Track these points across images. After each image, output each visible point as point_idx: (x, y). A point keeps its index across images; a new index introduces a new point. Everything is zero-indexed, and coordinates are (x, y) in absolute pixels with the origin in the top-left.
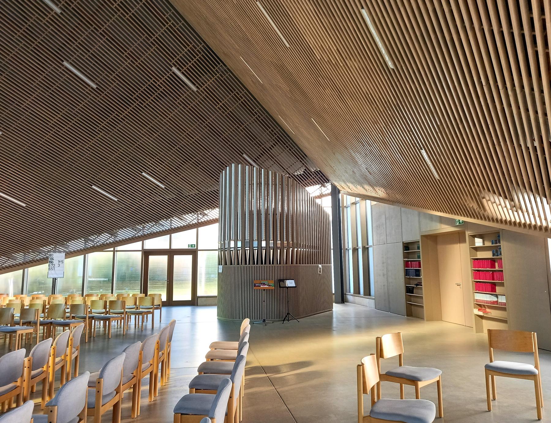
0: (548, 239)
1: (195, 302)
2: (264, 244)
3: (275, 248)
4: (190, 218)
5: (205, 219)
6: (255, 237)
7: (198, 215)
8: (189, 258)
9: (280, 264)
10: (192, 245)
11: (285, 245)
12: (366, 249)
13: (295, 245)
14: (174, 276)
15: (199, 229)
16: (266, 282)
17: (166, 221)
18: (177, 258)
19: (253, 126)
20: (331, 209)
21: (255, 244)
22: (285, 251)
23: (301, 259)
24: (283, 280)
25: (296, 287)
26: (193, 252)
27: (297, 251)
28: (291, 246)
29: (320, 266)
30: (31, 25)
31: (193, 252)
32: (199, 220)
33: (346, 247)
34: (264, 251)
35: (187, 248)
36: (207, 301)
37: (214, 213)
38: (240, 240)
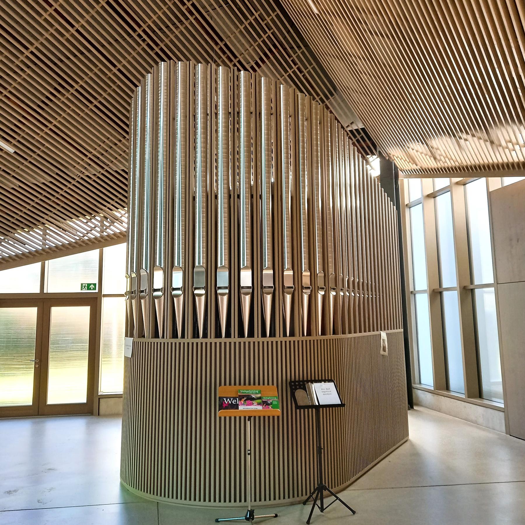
1: (92, 408)
2: (246, 278)
4: (81, 227)
6: (222, 259)
8: (83, 312)
9: (292, 334)
10: (89, 285)
11: (306, 281)
12: (468, 293)
13: (332, 284)
15: (106, 249)
16: (253, 392)
18: (57, 313)
19: (218, 14)
20: (437, 180)
23: (341, 322)
24: (300, 384)
25: (342, 405)
26: (91, 299)
28: (320, 282)
29: (384, 335)
31: (91, 299)
33: (411, 289)
34: (248, 298)
35: (79, 290)
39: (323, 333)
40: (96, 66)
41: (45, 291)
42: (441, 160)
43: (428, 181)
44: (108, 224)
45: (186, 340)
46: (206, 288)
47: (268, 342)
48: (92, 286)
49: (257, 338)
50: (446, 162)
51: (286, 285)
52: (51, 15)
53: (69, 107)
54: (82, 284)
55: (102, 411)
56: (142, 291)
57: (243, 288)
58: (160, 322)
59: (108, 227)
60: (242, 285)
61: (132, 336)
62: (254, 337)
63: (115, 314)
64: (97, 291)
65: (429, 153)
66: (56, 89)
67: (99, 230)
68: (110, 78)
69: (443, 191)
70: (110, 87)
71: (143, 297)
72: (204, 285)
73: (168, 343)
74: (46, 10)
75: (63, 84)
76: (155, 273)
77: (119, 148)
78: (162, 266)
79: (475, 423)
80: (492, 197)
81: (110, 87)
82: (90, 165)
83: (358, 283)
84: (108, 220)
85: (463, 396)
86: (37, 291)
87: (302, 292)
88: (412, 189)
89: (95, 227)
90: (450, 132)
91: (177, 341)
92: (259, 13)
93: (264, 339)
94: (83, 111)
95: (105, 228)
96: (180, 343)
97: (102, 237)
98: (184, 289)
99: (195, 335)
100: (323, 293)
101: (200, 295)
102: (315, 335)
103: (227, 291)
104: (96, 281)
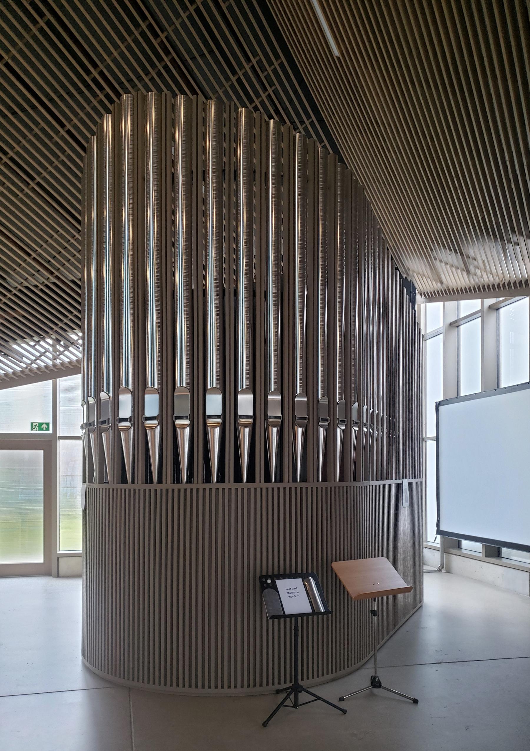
0: (277, 581)
1: (51, 568)
2: (245, 403)
10: (41, 424)
17: (33, 347)
20: (463, 303)
21: (214, 404)
22: (321, 430)
27: (358, 433)
29: (406, 482)
30: (18, 56)
38: (214, 391)
39: (342, 479)
40: (37, 124)
42: (475, 275)
44: (62, 349)
45: (163, 486)
46: (191, 417)
47: (273, 489)
48: (44, 426)
49: (260, 483)
50: (482, 277)
51: (298, 415)
54: (32, 423)
55: (61, 572)
56: (104, 422)
57: (241, 417)
59: (61, 353)
60: (240, 413)
61: (91, 481)
62: (255, 482)
63: (71, 457)
64: (51, 432)
65: (463, 266)
67: (51, 356)
68: (56, 144)
69: (470, 317)
71: (106, 430)
72: (188, 413)
78: (130, 387)
79: (493, 586)
84: (62, 343)
85: (480, 555)
86: (528, 573)
87: (318, 424)
88: (432, 315)
89: (45, 352)
91: (152, 487)
92: (258, 58)
93: (268, 485)
94: (22, 191)
95: (58, 353)
96: (156, 490)
97: (54, 365)
98: (160, 418)
99: (177, 479)
100: (343, 427)
101: (183, 427)
102: (333, 480)
103: (220, 421)
104: (50, 421)
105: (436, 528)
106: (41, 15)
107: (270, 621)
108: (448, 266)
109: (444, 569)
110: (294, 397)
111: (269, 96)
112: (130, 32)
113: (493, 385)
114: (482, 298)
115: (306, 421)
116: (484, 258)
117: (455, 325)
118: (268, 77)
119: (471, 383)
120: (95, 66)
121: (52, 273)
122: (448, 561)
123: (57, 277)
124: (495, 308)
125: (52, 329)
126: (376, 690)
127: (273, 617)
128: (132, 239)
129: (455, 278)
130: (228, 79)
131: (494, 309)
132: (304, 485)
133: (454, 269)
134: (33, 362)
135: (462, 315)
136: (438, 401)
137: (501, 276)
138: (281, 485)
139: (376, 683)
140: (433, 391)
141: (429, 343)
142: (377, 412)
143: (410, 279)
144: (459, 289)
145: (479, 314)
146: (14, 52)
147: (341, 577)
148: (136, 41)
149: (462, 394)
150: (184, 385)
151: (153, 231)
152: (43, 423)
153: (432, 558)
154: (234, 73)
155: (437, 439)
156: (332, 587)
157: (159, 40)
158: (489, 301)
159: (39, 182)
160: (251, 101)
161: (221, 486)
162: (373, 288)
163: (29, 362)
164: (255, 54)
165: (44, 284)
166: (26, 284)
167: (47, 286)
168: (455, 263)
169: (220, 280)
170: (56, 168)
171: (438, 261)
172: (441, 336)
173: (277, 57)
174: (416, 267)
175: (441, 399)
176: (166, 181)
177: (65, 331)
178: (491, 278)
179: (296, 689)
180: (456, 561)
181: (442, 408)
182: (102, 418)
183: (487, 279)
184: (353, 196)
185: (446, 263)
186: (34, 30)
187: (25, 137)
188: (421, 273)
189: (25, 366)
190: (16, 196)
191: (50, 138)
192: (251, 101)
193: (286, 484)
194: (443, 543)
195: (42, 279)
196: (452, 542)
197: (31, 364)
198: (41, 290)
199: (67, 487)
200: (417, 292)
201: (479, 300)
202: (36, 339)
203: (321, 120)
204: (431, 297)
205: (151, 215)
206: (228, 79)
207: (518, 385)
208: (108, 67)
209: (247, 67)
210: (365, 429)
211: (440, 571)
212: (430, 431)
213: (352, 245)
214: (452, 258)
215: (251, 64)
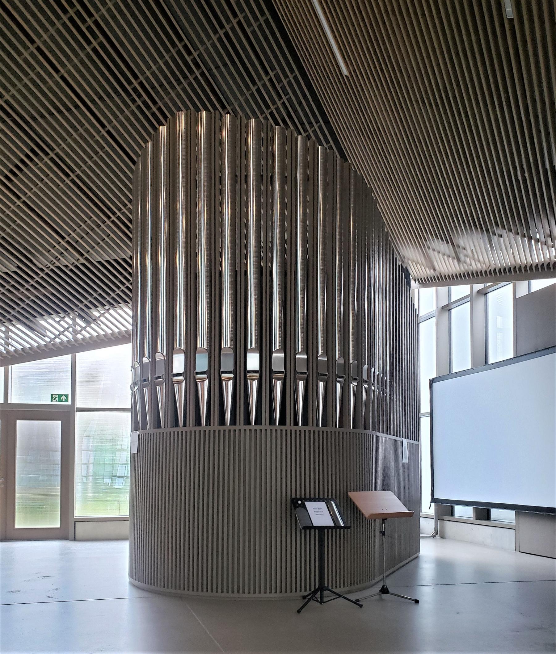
2: (253, 362)
3: (289, 377)
4: (55, 327)
5: (93, 331)
7: (73, 320)
10: (60, 396)
14: (128, 498)
17: (58, 323)
19: (222, 74)
20: (454, 288)
24: (296, 504)
26: (63, 413)
27: (368, 389)
29: (405, 441)
32: (76, 332)
36: (102, 530)
37: (120, 318)
38: (253, 350)
40: (82, 125)
41: (9, 402)
42: (465, 262)
43: (443, 290)
45: (211, 428)
46: (235, 372)
50: (471, 265)
52: (32, 55)
53: (47, 176)
54: (52, 395)
58: (181, 410)
60: (274, 369)
64: (69, 403)
66: (32, 151)
68: (97, 142)
69: (461, 301)
70: (96, 153)
71: (160, 384)
72: (232, 369)
73: (191, 431)
74: (27, 48)
75: (39, 148)
76: (174, 356)
77: (103, 231)
78: (183, 347)
79: (483, 545)
80: (519, 304)
81: (96, 153)
82: (66, 250)
83: (386, 381)
87: (336, 380)
88: (426, 299)
90: (483, 227)
92: (275, 72)
93: (296, 428)
98: (208, 372)
100: (356, 384)
104: (69, 392)
105: (430, 497)
106: (95, 37)
107: (303, 531)
108: (441, 255)
109: (439, 534)
110: (317, 357)
111: (284, 103)
112: (168, 51)
113: (482, 361)
114: (472, 283)
115: (326, 377)
116: (473, 248)
117: (447, 309)
118: (283, 88)
119: (462, 360)
120: (136, 77)
121: (82, 255)
122: (442, 528)
123: (86, 259)
124: (483, 293)
125: (77, 306)
126: (384, 596)
127: (305, 528)
128: (186, 227)
129: (446, 265)
130: (248, 88)
131: (482, 294)
132: (325, 429)
133: (446, 257)
134: (57, 336)
135: (453, 299)
136: (431, 378)
137: (488, 264)
138: (306, 428)
139: (384, 591)
140: (427, 370)
141: (423, 327)
142: (382, 375)
143: (405, 266)
144: (450, 275)
145: (469, 299)
146: (69, 67)
147: (357, 503)
148: (247, 101)
149: (454, 370)
150: (229, 346)
151: (204, 220)
152: (62, 395)
153: (427, 526)
154: (254, 83)
155: (431, 415)
156: (350, 509)
157: (192, 57)
158: (481, 286)
159: (78, 174)
160: (305, 130)
161: (258, 427)
162: (378, 273)
163: (53, 336)
164: (273, 68)
165: (74, 265)
166: (58, 264)
167: (76, 267)
168: (447, 252)
169: (233, 264)
170: (96, 163)
171: (431, 251)
172: (434, 319)
173: (292, 71)
174: (410, 255)
175: (434, 376)
176: (215, 181)
177: (35, 317)
178: (479, 265)
179: (322, 588)
180: (450, 527)
181: (435, 385)
182: (150, 376)
183: (476, 266)
184: (364, 194)
185: (439, 252)
186: (89, 49)
187: (70, 135)
188: (415, 259)
189: (48, 340)
190: (58, 186)
191: (93, 137)
192: (305, 130)
193: (310, 427)
194: (437, 511)
195: (70, 260)
196: (445, 509)
197: (55, 338)
198: (71, 270)
199: (89, 450)
200: (411, 278)
201: (469, 286)
202: (62, 315)
203: (327, 122)
204: (425, 282)
205: (180, 206)
206: (248, 88)
207: (503, 361)
208: (147, 79)
209: (266, 79)
210: (373, 388)
211: (434, 536)
212: (424, 407)
213: (362, 235)
214: (444, 247)
215: (269, 77)
